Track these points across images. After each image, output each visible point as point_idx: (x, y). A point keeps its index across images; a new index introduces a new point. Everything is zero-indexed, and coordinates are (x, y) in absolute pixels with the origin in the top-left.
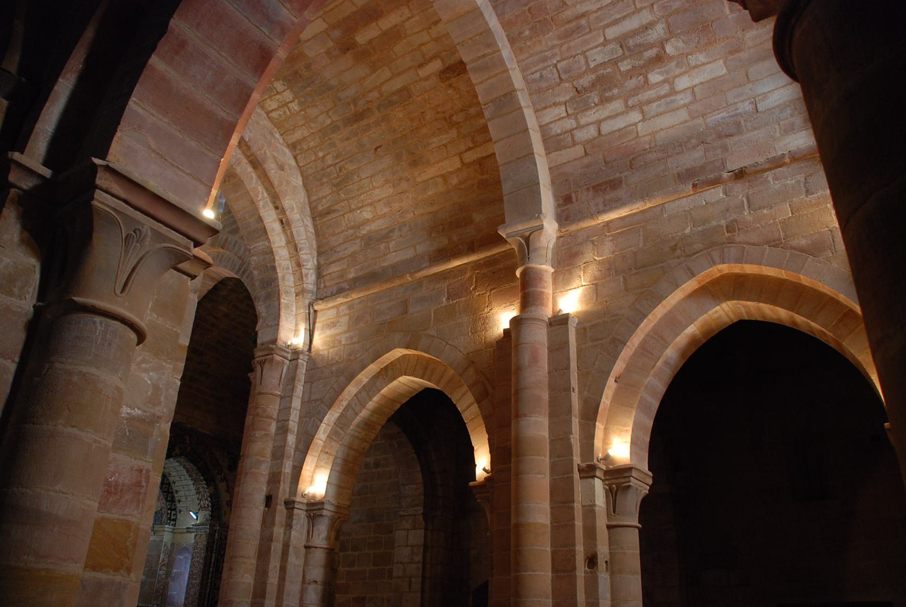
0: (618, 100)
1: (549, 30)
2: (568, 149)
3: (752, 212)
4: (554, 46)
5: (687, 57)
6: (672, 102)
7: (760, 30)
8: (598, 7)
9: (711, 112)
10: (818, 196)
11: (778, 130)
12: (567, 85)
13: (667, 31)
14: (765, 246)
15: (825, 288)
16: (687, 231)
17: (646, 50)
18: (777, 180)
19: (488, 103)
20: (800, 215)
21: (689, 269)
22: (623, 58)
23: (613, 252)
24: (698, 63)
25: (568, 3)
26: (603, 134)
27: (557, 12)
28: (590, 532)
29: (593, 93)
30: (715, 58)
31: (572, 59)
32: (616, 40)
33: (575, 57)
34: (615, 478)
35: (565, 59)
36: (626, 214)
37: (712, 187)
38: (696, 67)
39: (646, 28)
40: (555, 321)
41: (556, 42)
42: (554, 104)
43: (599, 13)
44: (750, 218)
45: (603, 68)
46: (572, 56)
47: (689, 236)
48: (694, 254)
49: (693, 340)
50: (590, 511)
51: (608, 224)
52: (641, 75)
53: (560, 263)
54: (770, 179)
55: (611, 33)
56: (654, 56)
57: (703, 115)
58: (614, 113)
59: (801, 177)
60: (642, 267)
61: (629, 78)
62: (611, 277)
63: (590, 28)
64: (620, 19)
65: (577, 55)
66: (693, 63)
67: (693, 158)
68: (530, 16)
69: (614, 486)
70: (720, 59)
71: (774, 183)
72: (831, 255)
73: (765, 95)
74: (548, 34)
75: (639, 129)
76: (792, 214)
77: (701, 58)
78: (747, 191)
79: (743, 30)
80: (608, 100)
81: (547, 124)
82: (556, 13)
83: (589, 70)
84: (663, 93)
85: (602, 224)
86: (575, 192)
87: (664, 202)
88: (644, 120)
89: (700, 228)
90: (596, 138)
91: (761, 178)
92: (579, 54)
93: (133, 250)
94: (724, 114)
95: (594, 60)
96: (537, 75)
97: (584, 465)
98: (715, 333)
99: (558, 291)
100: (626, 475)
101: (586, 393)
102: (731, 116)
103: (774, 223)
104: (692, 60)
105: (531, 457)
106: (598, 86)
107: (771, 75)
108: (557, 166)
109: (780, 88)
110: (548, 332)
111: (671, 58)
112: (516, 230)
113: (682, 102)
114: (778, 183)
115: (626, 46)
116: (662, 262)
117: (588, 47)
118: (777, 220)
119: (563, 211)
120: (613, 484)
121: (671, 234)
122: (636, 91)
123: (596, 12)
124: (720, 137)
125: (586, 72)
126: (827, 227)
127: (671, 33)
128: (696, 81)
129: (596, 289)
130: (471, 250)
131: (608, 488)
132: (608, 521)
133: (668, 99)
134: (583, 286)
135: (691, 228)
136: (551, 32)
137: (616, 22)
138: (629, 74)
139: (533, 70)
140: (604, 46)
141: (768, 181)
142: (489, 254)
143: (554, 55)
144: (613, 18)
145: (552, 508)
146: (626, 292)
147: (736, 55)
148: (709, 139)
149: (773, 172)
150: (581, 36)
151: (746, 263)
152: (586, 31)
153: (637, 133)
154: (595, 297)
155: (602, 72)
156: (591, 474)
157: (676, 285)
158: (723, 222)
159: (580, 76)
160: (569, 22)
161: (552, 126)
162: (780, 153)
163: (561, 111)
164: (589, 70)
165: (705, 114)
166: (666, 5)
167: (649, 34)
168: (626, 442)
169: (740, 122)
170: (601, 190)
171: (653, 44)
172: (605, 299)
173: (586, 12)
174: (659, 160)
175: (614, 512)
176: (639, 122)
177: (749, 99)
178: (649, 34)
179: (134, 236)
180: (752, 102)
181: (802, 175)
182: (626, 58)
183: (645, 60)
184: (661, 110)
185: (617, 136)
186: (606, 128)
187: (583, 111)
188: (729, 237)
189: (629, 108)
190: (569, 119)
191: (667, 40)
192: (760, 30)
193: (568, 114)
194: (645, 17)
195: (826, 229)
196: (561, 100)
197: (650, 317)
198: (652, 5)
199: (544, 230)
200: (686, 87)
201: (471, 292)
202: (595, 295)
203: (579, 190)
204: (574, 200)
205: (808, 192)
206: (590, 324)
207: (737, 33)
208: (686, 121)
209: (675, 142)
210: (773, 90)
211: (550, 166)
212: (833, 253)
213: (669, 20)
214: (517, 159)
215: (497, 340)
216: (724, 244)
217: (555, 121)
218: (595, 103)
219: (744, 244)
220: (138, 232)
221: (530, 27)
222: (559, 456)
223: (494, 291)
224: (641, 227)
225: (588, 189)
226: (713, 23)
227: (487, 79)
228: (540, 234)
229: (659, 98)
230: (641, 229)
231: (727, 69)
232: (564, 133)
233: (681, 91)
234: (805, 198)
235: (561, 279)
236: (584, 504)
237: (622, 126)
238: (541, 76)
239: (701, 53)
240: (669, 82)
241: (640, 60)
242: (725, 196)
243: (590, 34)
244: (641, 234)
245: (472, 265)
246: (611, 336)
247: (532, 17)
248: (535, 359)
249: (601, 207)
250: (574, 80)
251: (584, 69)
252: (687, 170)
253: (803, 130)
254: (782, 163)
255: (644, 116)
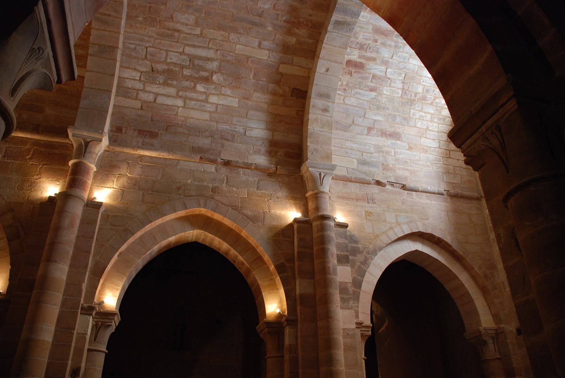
0: (174, 88)
1: (154, 26)
2: (131, 100)
3: (227, 186)
4: (152, 36)
5: (221, 87)
6: (204, 106)
7: (262, 95)
8: (189, 32)
9: (222, 123)
10: (262, 192)
11: (252, 150)
12: (148, 63)
13: (218, 68)
14: (229, 208)
15: (253, 241)
16: (189, 181)
17: (203, 71)
18: (245, 175)
19: (95, 44)
20: (251, 198)
21: (185, 204)
22: (188, 67)
23: (140, 175)
24: (225, 93)
25: (174, 19)
26: (157, 102)
27: (165, 20)
28: (79, 352)
29: (161, 76)
30: (235, 96)
31: (159, 50)
32: (189, 55)
33: (161, 50)
34: (102, 318)
35: (154, 48)
36: (155, 156)
37: (210, 163)
38: (224, 95)
39: (208, 59)
40: (91, 204)
41: (154, 35)
42: (134, 68)
43: (188, 36)
44: (225, 189)
45: (173, 66)
46: (159, 49)
47: (190, 185)
48: (189, 196)
49: (169, 245)
50: (82, 337)
51: (142, 156)
52: (193, 82)
53: (102, 167)
54: (241, 173)
55: (188, 50)
56: (205, 76)
57: (217, 122)
58: (169, 94)
59: (257, 179)
60: (156, 191)
61: (186, 80)
62: (135, 190)
63: (178, 40)
64: (197, 46)
65: (163, 50)
66: (223, 92)
67: (204, 142)
68: (148, 11)
69: (100, 323)
70: (237, 98)
71: (243, 176)
72: (261, 225)
73: (252, 129)
74: (153, 27)
75: (179, 111)
76: (248, 196)
77: (229, 92)
78: (228, 174)
79: (254, 91)
80: (169, 85)
81: (124, 78)
82: (164, 19)
83: (165, 62)
84: (201, 98)
85: (137, 155)
86: (125, 127)
87: (180, 159)
88: (184, 107)
89: (197, 183)
90: (152, 102)
91: (237, 170)
92: (164, 50)
93: (30, 63)
94: (228, 127)
95: (171, 59)
96: (133, 46)
97: (86, 305)
98: (181, 244)
99: (95, 185)
100: (111, 317)
101: (98, 257)
102: (232, 130)
103: (237, 197)
104: (224, 90)
105: (52, 292)
106: (166, 74)
107: (259, 120)
108: (119, 106)
109: (260, 129)
110: (83, 209)
111: (213, 83)
112: (81, 133)
113: (209, 109)
114: (245, 177)
115: (193, 62)
116: (169, 194)
117: (171, 49)
118: (239, 196)
119: (113, 135)
120: (99, 322)
121: (180, 179)
122: (186, 89)
123: (186, 34)
124: (222, 138)
125: (163, 62)
126: (263, 210)
127: (219, 70)
128: (221, 102)
129: (123, 194)
130: (36, 130)
131: (95, 323)
132: (89, 346)
133: (202, 103)
134: (114, 188)
135: (192, 181)
136: (155, 28)
137: (194, 46)
138: (187, 78)
139: (132, 42)
140: (181, 55)
141: (240, 174)
142: (50, 139)
143: (149, 41)
144: (194, 43)
145: (56, 331)
146: (142, 203)
147: (246, 101)
148: (216, 137)
149: (244, 170)
150: (171, 41)
151: (217, 213)
152: (175, 40)
153: (177, 112)
154: (120, 198)
155: (172, 67)
156: (89, 313)
157: (175, 210)
158: (210, 185)
159: (159, 62)
160: (169, 29)
161: (127, 81)
162: (250, 162)
163: (137, 75)
164: (165, 62)
165: (219, 122)
166: (225, 54)
167: (208, 64)
168: (115, 296)
169: (235, 136)
170: (143, 134)
171: (208, 70)
172: (127, 202)
173: (181, 30)
174: (184, 134)
175: (95, 340)
176: (181, 107)
177: (243, 126)
178: (208, 64)
179: (37, 53)
180: (244, 129)
181: (258, 178)
182: (189, 68)
183: (199, 76)
184: (196, 107)
185: (165, 108)
186: (160, 100)
187: (150, 83)
188: (212, 194)
189: (177, 96)
190: (139, 82)
191: (216, 73)
192: (262, 95)
193: (140, 79)
194: (211, 54)
195: (262, 211)
196: (140, 69)
197: (153, 223)
198: (218, 50)
199: (102, 142)
200: (214, 102)
201: (26, 160)
202: (121, 197)
203: (129, 127)
204: (124, 132)
205: (258, 188)
206: (113, 214)
207: (251, 90)
208: (206, 120)
209: (197, 129)
210: (257, 128)
211: (115, 104)
212: (262, 225)
213: (222, 63)
214: (99, 89)
215: (41, 201)
216: (208, 197)
217: (130, 79)
218: (159, 82)
219: (219, 202)
220: (41, 52)
221: (145, 17)
222: (70, 296)
223: (47, 166)
224: (162, 167)
225: (135, 130)
226: (242, 78)
227: (104, 30)
228: (98, 144)
229: (197, 100)
230: (161, 169)
231: (238, 105)
232: (133, 89)
233: (211, 103)
234: (256, 191)
235: (100, 177)
236: (78, 332)
237: (170, 104)
238: (135, 48)
239: (230, 90)
240: (206, 95)
241: (197, 74)
242: (215, 171)
243: (176, 44)
244: (161, 172)
245: (34, 141)
246: (125, 227)
247: (149, 12)
248: (72, 225)
249: (140, 145)
250: (153, 62)
251: (163, 60)
252: (198, 147)
253: (264, 156)
254: (250, 168)
255: (185, 105)
